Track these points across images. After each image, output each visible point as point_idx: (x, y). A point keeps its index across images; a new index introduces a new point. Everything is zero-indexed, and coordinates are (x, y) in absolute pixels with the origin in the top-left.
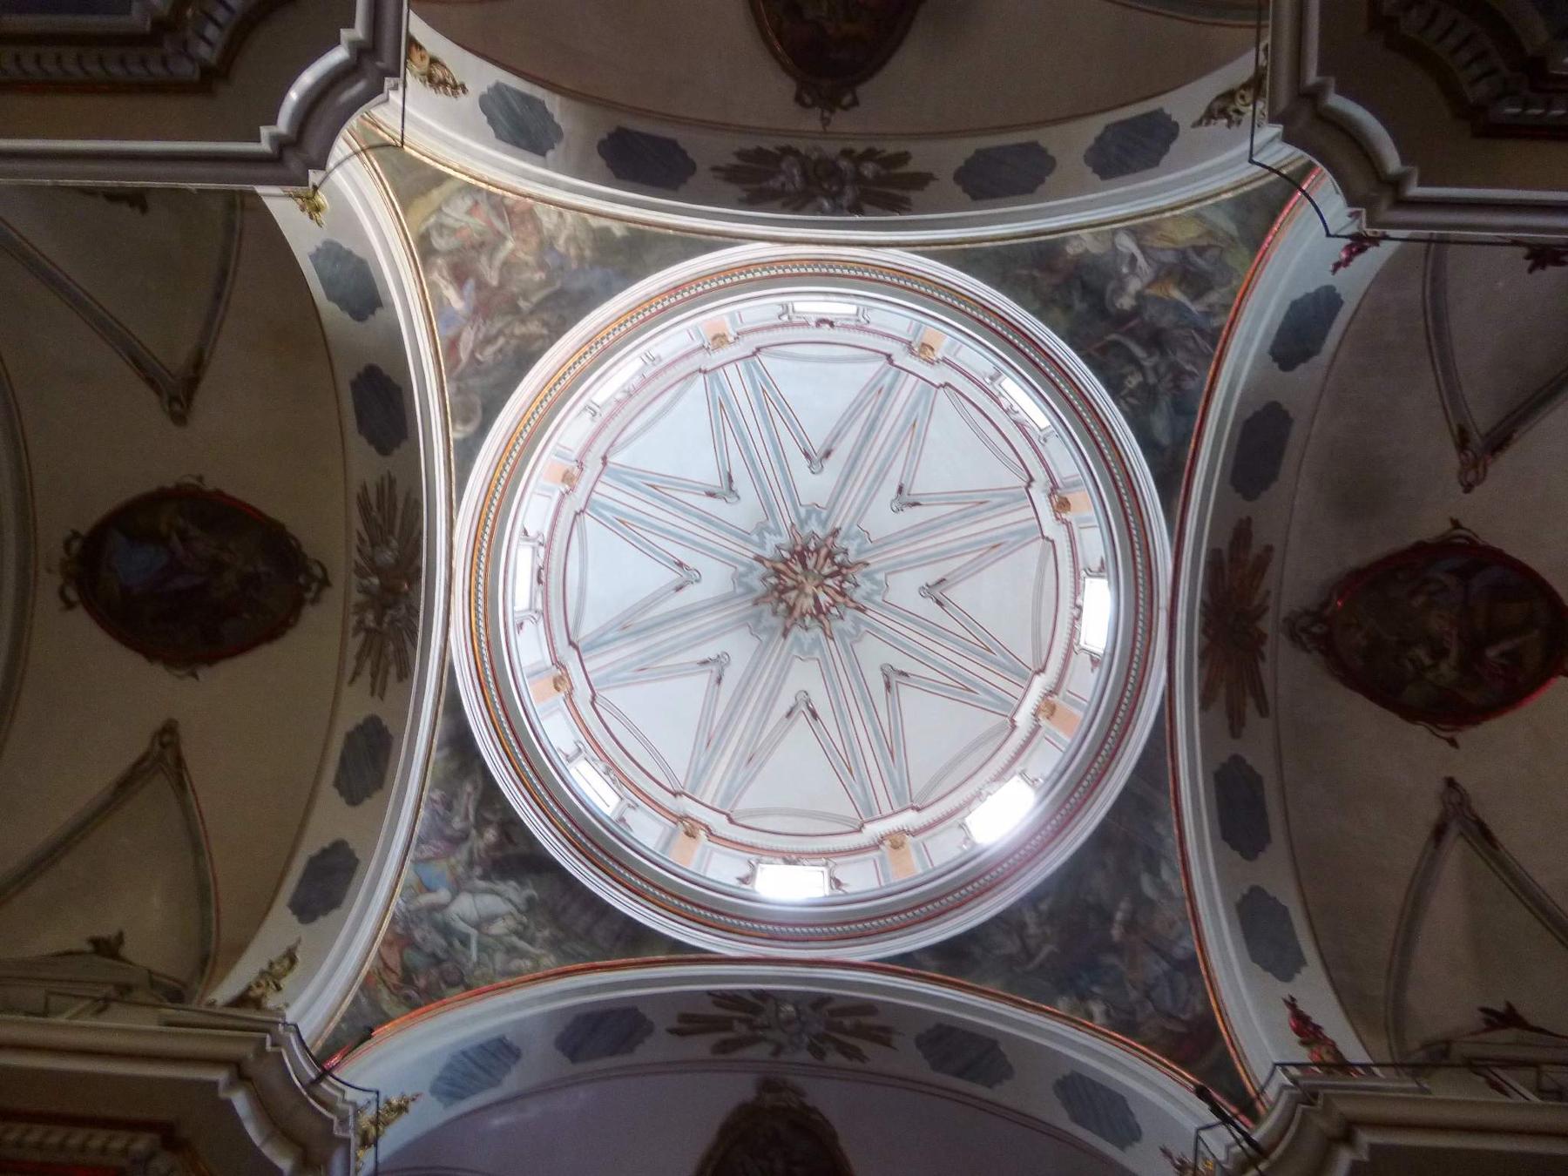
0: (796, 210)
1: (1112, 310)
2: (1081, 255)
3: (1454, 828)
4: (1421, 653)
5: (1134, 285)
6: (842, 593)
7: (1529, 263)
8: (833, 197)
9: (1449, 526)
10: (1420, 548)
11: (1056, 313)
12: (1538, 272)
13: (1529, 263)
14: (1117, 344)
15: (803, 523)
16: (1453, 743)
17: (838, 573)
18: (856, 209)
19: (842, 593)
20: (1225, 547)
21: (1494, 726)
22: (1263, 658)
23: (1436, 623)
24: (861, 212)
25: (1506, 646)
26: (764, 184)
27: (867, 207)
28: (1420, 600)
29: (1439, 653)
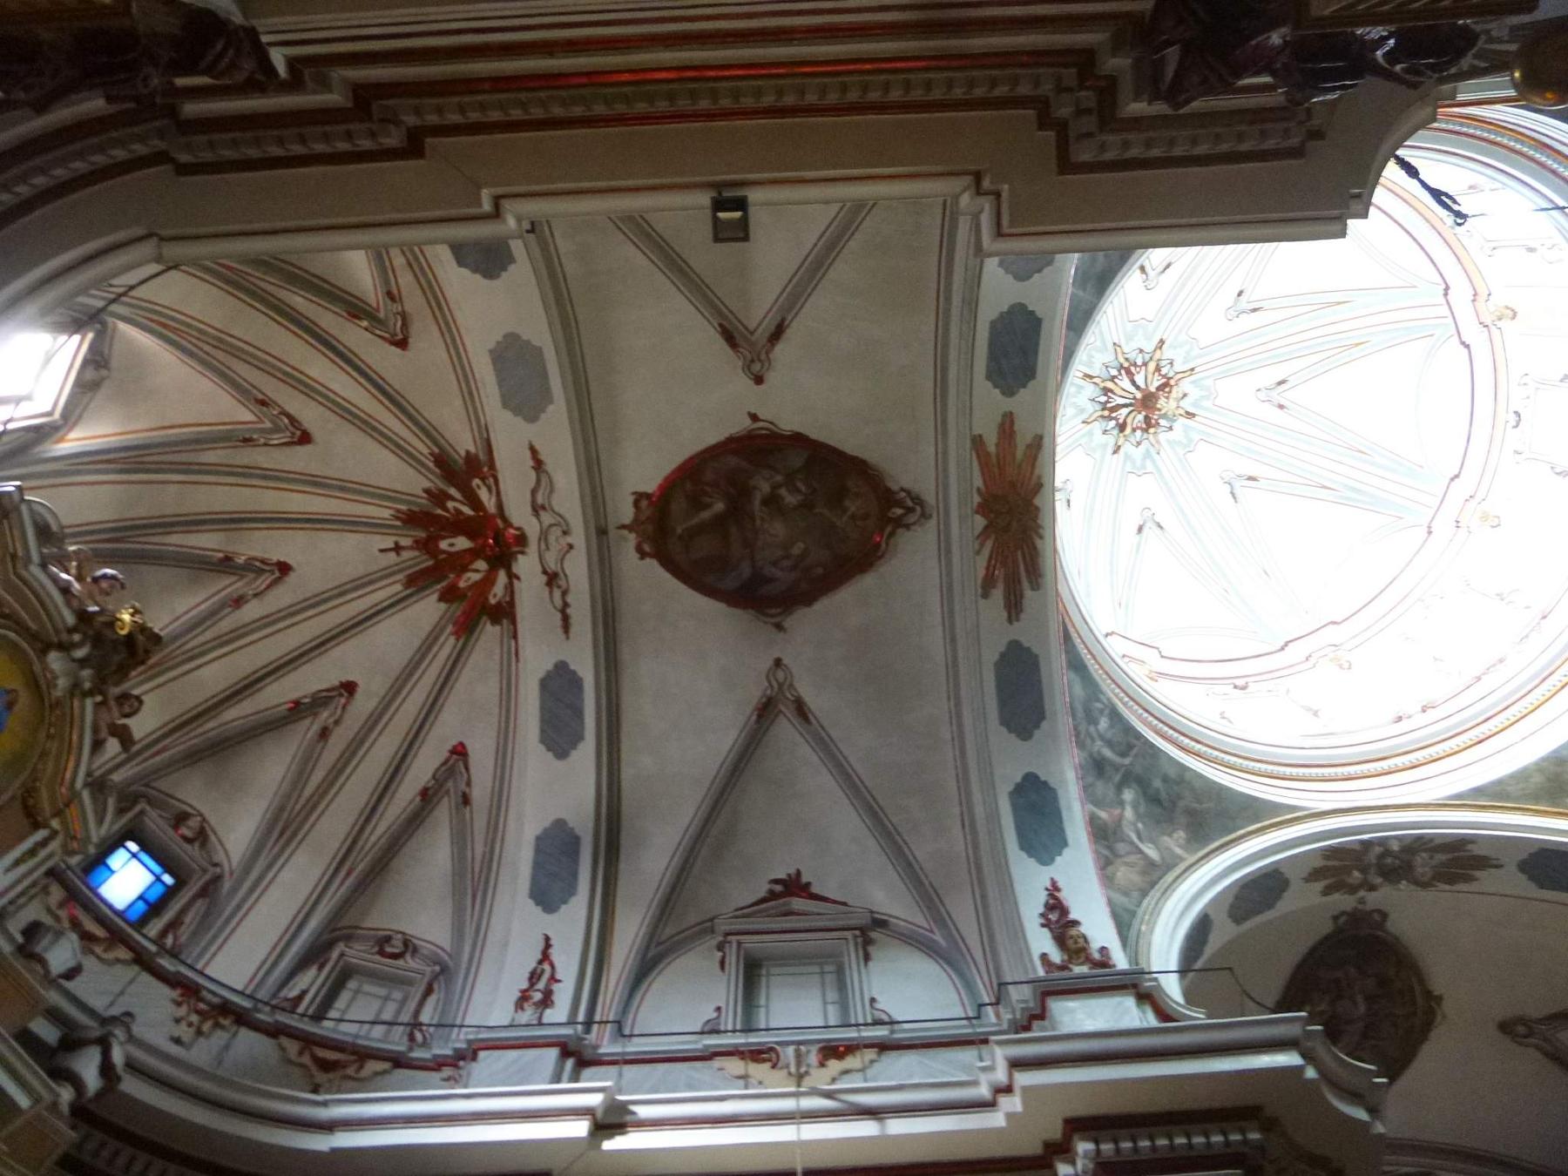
0: (1420, 838)
1: (1134, 785)
2: (1174, 831)
3: (761, 336)
4: (790, 499)
5: (1129, 813)
6: (1106, 391)
7: (804, 879)
8: (1387, 853)
9: (786, 624)
10: (808, 599)
11: (1172, 772)
12: (792, 871)
13: (804, 879)
14: (1123, 755)
15: (1147, 455)
16: (754, 417)
17: (1113, 410)
18: (1367, 844)
19: (1106, 391)
20: (1028, 593)
21: (713, 437)
22: (978, 490)
23: (778, 529)
24: (1362, 842)
25: (706, 515)
26: (1450, 856)
27: (1357, 847)
28: (797, 549)
29: (772, 501)
